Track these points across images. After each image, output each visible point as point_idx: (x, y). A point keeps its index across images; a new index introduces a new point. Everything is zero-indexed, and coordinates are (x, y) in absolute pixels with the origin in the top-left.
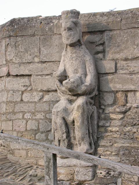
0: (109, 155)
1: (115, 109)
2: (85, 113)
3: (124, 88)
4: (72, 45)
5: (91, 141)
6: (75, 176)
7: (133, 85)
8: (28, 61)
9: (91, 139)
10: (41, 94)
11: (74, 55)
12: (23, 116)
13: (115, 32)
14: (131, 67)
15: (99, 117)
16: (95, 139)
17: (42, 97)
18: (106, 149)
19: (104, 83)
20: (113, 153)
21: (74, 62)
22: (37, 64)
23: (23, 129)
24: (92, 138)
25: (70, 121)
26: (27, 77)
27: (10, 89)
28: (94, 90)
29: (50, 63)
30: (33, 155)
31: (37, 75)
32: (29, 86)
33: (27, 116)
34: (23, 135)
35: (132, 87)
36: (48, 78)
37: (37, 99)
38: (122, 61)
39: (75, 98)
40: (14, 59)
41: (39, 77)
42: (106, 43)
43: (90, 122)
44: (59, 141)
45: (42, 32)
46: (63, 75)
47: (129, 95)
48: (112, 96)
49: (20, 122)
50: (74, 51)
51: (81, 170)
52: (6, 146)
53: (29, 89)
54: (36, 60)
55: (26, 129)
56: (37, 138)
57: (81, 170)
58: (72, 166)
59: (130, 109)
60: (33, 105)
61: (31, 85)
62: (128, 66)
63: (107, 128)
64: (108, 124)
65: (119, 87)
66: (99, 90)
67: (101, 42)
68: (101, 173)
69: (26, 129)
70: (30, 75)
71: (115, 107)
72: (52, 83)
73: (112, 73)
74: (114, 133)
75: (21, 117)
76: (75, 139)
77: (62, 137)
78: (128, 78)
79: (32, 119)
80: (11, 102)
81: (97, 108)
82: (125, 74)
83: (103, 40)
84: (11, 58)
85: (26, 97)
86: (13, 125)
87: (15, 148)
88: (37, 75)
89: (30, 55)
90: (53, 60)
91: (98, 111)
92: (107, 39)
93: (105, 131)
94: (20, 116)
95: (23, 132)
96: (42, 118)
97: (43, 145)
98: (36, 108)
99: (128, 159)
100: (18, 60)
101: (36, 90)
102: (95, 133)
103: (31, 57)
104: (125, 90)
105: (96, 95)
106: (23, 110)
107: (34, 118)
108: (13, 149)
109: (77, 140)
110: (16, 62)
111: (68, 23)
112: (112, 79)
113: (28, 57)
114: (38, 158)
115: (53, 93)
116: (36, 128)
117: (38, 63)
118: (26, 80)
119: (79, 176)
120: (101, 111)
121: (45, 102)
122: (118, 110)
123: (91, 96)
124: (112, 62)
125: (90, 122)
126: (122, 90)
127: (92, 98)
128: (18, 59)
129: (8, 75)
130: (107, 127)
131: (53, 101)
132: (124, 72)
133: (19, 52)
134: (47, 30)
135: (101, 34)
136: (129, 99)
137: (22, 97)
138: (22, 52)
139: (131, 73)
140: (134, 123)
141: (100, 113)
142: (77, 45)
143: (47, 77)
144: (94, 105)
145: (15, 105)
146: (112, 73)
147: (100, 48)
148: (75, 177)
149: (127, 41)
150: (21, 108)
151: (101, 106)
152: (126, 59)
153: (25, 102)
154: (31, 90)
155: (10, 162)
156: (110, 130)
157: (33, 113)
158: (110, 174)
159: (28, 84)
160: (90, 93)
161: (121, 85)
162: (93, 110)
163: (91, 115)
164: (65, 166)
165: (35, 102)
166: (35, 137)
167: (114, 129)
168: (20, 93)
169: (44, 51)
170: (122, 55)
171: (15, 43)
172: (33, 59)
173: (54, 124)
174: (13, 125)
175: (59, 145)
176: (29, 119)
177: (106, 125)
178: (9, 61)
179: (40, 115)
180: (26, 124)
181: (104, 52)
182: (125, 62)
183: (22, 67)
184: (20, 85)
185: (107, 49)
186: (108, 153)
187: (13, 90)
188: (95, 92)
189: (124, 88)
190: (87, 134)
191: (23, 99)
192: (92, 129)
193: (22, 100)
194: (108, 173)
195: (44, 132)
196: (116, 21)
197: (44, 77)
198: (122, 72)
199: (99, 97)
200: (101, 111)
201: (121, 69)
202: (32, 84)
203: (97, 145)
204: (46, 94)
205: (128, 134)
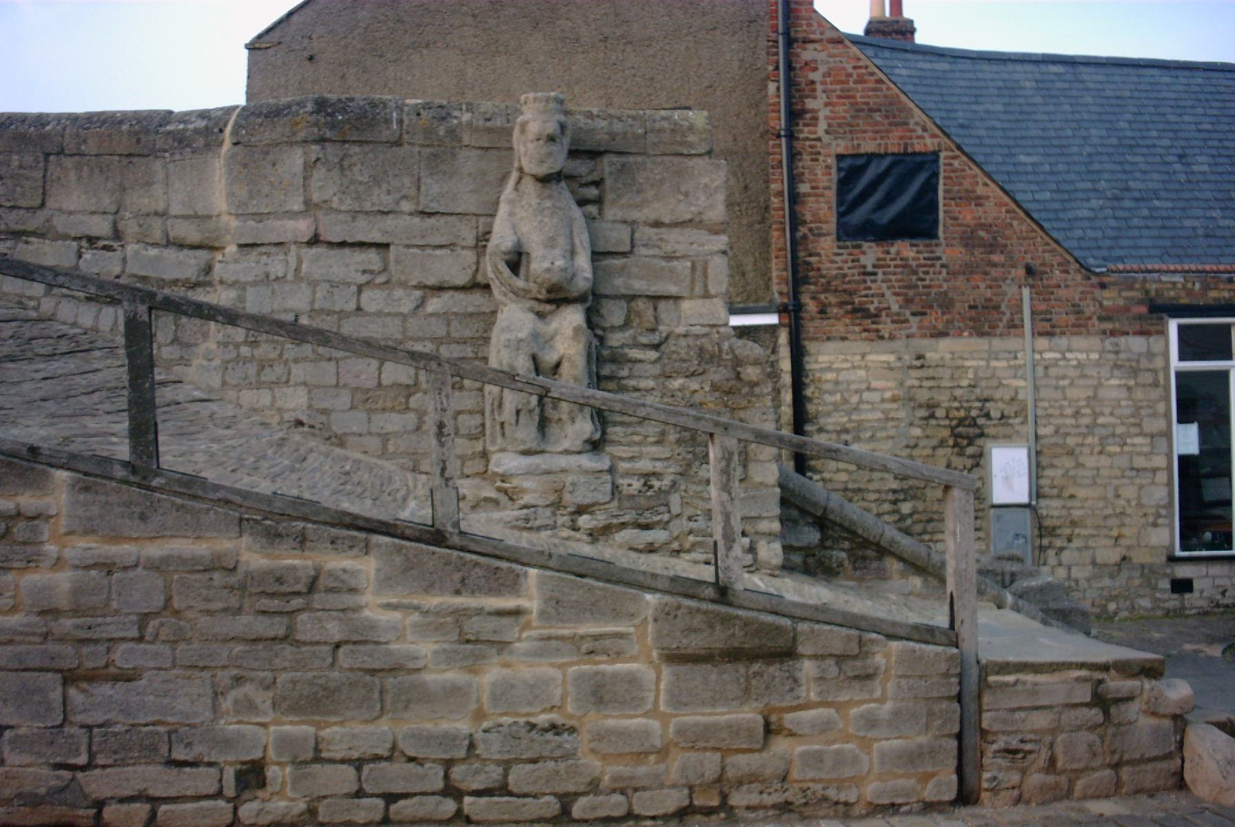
0: (640, 444)
1: (634, 338)
3: (653, 288)
4: (544, 180)
7: (675, 284)
8: (382, 209)
10: (418, 293)
11: (548, 203)
13: (631, 159)
17: (422, 303)
18: (630, 430)
20: (651, 439)
21: (546, 220)
22: (408, 218)
23: (372, 383)
26: (373, 250)
29: (450, 219)
30: (401, 449)
31: (408, 246)
32: (380, 273)
35: (673, 289)
37: (407, 307)
40: (335, 199)
41: (415, 250)
42: (609, 182)
45: (426, 138)
47: (662, 305)
50: (547, 192)
52: (318, 426)
53: (380, 279)
54: (406, 206)
58: (555, 473)
59: (667, 338)
61: (385, 269)
62: (661, 239)
63: (624, 382)
64: (624, 373)
65: (639, 286)
67: (595, 176)
68: (630, 485)
70: (386, 246)
73: (624, 254)
77: (529, 402)
78: (663, 268)
82: (654, 256)
84: (326, 198)
86: (338, 373)
87: (347, 430)
88: (408, 246)
89: (389, 192)
90: (459, 210)
92: (611, 173)
95: (369, 390)
97: (712, 420)
100: (348, 205)
101: (403, 285)
108: (339, 432)
110: (343, 208)
111: (549, 124)
112: (623, 268)
113: (380, 198)
115: (451, 293)
116: (411, 382)
117: (411, 214)
121: (431, 315)
124: (623, 227)
128: (349, 201)
129: (315, 241)
131: (456, 314)
132: (651, 252)
133: (352, 182)
134: (442, 133)
135: (592, 159)
136: (664, 316)
137: (358, 300)
138: (361, 183)
139: (669, 258)
140: (692, 369)
143: (438, 252)
145: (340, 319)
146: (624, 254)
147: (593, 192)
149: (662, 181)
152: (657, 224)
153: (367, 314)
154: (386, 283)
158: (651, 487)
159: (377, 266)
161: (644, 282)
165: (404, 317)
166: (407, 402)
167: (643, 384)
168: (354, 289)
169: (432, 187)
170: (648, 213)
171: (342, 159)
172: (397, 203)
174: (338, 373)
175: (517, 421)
178: (317, 205)
180: (380, 369)
181: (599, 201)
183: (362, 222)
184: (352, 268)
185: (610, 196)
186: (637, 438)
191: (364, 304)
193: (359, 309)
194: (645, 484)
196: (634, 134)
197: (429, 251)
198: (644, 251)
201: (644, 245)
204: (433, 296)
205: (679, 394)
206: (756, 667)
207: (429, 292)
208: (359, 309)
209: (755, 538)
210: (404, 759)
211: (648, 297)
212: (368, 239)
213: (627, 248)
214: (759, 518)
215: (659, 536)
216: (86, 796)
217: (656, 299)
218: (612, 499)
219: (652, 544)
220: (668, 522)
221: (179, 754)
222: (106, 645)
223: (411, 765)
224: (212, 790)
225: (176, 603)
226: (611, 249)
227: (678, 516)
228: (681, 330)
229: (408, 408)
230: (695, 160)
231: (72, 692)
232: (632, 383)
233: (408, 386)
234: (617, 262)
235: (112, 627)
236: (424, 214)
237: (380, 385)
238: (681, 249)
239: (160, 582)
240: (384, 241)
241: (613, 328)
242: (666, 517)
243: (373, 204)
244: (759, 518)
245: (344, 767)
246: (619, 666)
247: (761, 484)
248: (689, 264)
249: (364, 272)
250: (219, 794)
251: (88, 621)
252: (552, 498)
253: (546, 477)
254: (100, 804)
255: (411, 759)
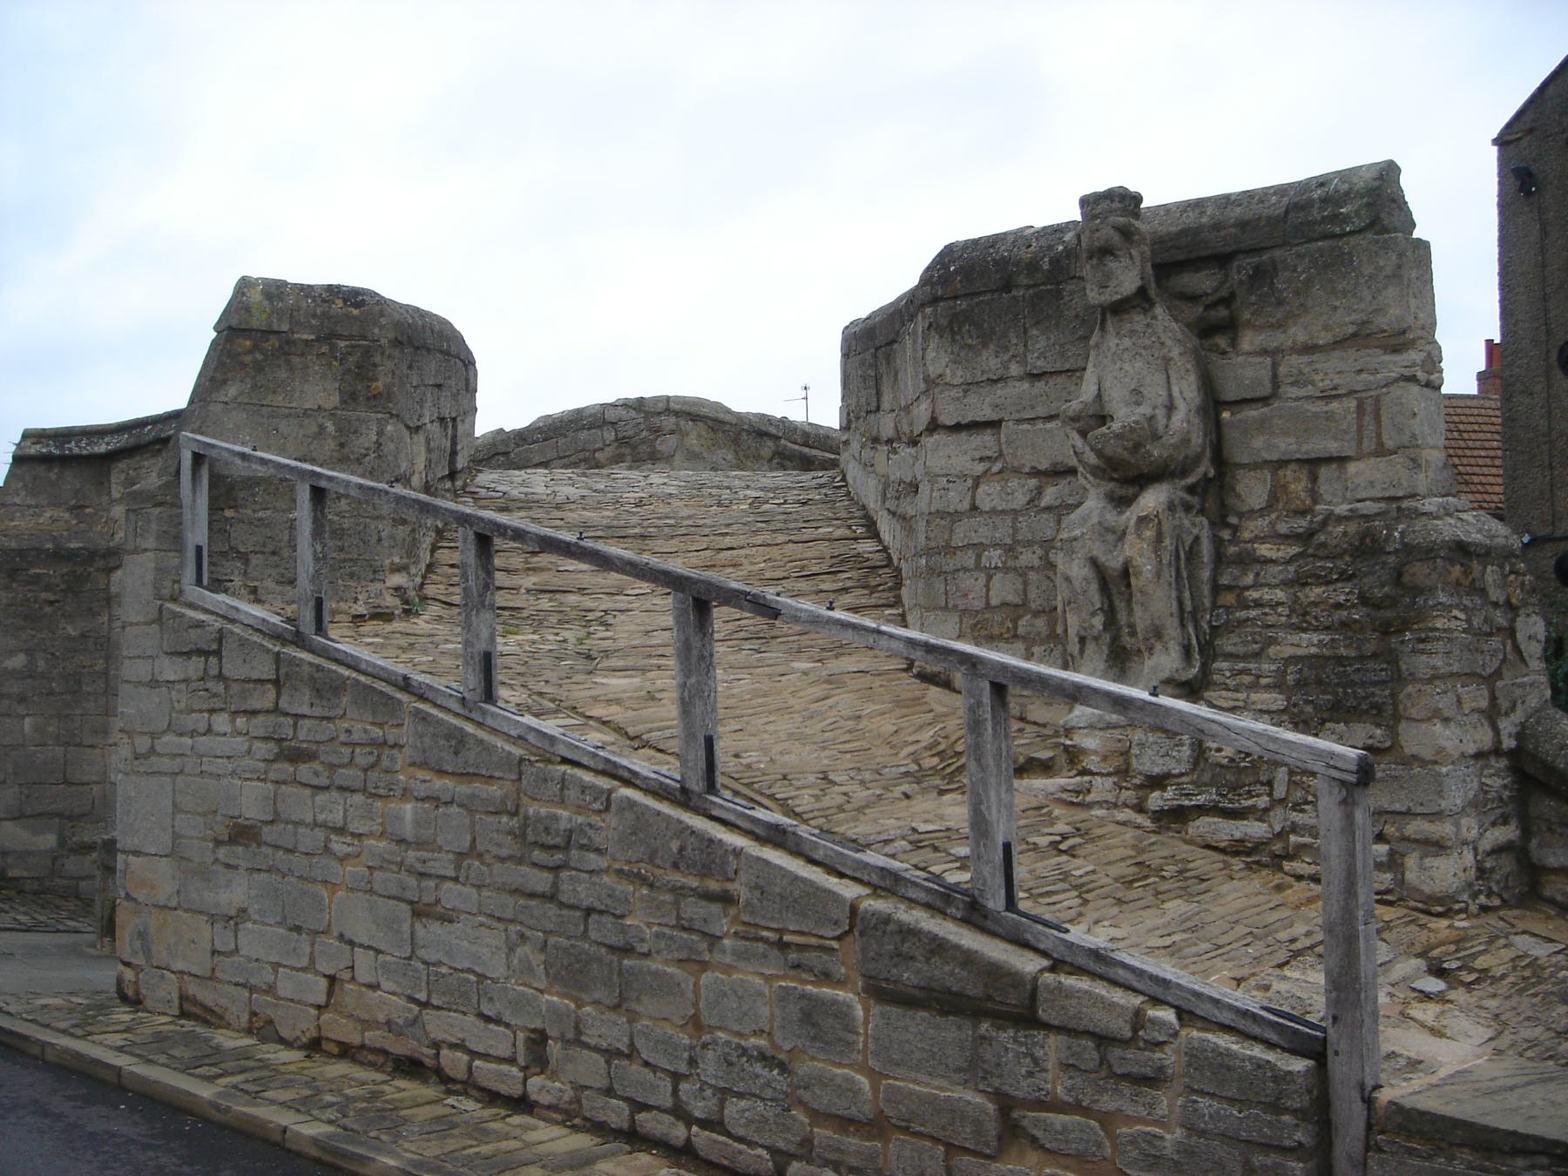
2: (1167, 542)
3: (1305, 447)
5: (1189, 640)
6: (1134, 761)
7: (1335, 439)
9: (1189, 635)
10: (1033, 482)
12: (979, 557)
14: (1326, 374)
15: (1219, 558)
16: (1205, 633)
17: (1039, 491)
19: (1112, 342)
20: (1264, 681)
22: (1018, 384)
23: (979, 604)
24: (1191, 630)
25: (1114, 569)
27: (937, 470)
28: (1197, 459)
32: (996, 459)
33: (994, 557)
34: (978, 623)
35: (1332, 447)
36: (1051, 430)
37: (1020, 499)
38: (1295, 356)
39: (1131, 491)
40: (948, 371)
41: (1026, 426)
43: (1185, 574)
44: (1082, 640)
46: (1091, 412)
48: (1265, 480)
49: (966, 581)
51: (1151, 739)
54: (1015, 369)
55: (988, 603)
56: (1021, 631)
57: (1151, 739)
60: (1008, 520)
61: (1001, 455)
63: (1247, 594)
64: (1249, 579)
65: (1285, 446)
66: (1220, 459)
67: (1224, 293)
69: (988, 603)
70: (995, 425)
71: (1273, 516)
72: (1063, 444)
73: (1264, 400)
74: (1267, 610)
75: (971, 563)
76: (1133, 634)
78: (1316, 415)
79: (1006, 569)
80: (941, 514)
81: (1212, 524)
82: (1307, 398)
83: (1228, 285)
84: (939, 371)
85: (989, 496)
88: (1019, 421)
91: (1214, 535)
93: (1239, 602)
94: (969, 559)
95: (977, 612)
96: (1036, 563)
98: (1016, 530)
99: (1312, 701)
101: (1017, 471)
102: (1204, 610)
103: (999, 360)
104: (1306, 457)
105: (1206, 480)
106: (980, 540)
107: (1010, 563)
109: (1140, 636)
114: (1024, 700)
116: (1017, 600)
117: (1020, 379)
118: (987, 437)
119: (1145, 759)
120: (1226, 534)
122: (1283, 528)
123: (1191, 480)
125: (1185, 574)
126: (1299, 456)
127: (1191, 490)
128: (960, 373)
129: (934, 426)
130: (1247, 588)
132: (1302, 392)
136: (1324, 488)
137: (973, 497)
141: (1222, 540)
142: (1134, 307)
143: (1049, 426)
144: (1202, 512)
148: (1134, 763)
149: (1309, 283)
150: (973, 534)
151: (1226, 516)
152: (1309, 349)
154: (1000, 472)
155: (932, 711)
156: (1255, 601)
157: (1010, 550)
160: (1184, 472)
161: (1292, 440)
162: (1195, 531)
163: (1191, 548)
164: (1101, 726)
165: (1015, 512)
166: (1016, 628)
167: (1266, 595)
168: (970, 481)
172: (1006, 368)
173: (1065, 585)
176: (996, 568)
177: (1241, 584)
179: (1030, 555)
180: (987, 586)
182: (1305, 359)
183: (972, 399)
186: (1247, 679)
187: (946, 475)
188: (1206, 468)
189: (1303, 450)
190: (1172, 615)
192: (1192, 599)
193: (974, 507)
195: (1044, 611)
198: (1294, 392)
199: (1222, 487)
200: (1226, 534)
201: (1292, 384)
202: (1005, 452)
203: (1209, 651)
206: (985, 1027)
207: (1043, 479)
208: (974, 507)
209: (1400, 847)
210: (640, 1062)
211: (1301, 462)
212: (979, 417)
213: (1265, 390)
214: (1409, 814)
215: (1254, 829)
216: (427, 1034)
217: (1313, 464)
218: (1193, 770)
219: (1241, 841)
220: (1266, 810)
221: (487, 1009)
222: (437, 881)
223: (646, 1071)
224: (507, 1053)
225: (480, 847)
226: (1245, 395)
227: (1282, 801)
228: (1342, 509)
229: (1016, 636)
230: (1353, 240)
231: (418, 926)
232: (1254, 594)
233: (1017, 606)
234: (1252, 413)
235: (437, 864)
236: (1034, 377)
237: (988, 606)
238: (1345, 382)
239: (467, 821)
240: (995, 417)
241: (1252, 513)
242: (1263, 802)
243: (983, 372)
244: (1409, 814)
245: (595, 1056)
246: (827, 991)
247: (1415, 757)
248: (1353, 404)
249: (982, 459)
250: (511, 1061)
251: (425, 855)
252: (1117, 762)
253: (1108, 734)
254: (436, 1045)
255: (647, 1064)
